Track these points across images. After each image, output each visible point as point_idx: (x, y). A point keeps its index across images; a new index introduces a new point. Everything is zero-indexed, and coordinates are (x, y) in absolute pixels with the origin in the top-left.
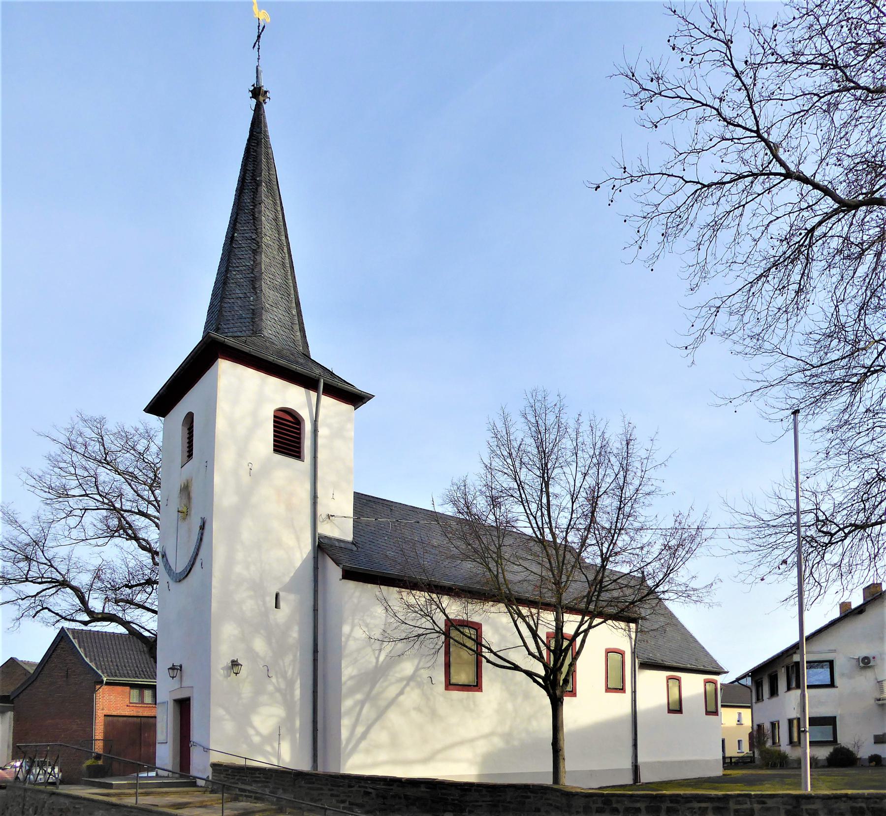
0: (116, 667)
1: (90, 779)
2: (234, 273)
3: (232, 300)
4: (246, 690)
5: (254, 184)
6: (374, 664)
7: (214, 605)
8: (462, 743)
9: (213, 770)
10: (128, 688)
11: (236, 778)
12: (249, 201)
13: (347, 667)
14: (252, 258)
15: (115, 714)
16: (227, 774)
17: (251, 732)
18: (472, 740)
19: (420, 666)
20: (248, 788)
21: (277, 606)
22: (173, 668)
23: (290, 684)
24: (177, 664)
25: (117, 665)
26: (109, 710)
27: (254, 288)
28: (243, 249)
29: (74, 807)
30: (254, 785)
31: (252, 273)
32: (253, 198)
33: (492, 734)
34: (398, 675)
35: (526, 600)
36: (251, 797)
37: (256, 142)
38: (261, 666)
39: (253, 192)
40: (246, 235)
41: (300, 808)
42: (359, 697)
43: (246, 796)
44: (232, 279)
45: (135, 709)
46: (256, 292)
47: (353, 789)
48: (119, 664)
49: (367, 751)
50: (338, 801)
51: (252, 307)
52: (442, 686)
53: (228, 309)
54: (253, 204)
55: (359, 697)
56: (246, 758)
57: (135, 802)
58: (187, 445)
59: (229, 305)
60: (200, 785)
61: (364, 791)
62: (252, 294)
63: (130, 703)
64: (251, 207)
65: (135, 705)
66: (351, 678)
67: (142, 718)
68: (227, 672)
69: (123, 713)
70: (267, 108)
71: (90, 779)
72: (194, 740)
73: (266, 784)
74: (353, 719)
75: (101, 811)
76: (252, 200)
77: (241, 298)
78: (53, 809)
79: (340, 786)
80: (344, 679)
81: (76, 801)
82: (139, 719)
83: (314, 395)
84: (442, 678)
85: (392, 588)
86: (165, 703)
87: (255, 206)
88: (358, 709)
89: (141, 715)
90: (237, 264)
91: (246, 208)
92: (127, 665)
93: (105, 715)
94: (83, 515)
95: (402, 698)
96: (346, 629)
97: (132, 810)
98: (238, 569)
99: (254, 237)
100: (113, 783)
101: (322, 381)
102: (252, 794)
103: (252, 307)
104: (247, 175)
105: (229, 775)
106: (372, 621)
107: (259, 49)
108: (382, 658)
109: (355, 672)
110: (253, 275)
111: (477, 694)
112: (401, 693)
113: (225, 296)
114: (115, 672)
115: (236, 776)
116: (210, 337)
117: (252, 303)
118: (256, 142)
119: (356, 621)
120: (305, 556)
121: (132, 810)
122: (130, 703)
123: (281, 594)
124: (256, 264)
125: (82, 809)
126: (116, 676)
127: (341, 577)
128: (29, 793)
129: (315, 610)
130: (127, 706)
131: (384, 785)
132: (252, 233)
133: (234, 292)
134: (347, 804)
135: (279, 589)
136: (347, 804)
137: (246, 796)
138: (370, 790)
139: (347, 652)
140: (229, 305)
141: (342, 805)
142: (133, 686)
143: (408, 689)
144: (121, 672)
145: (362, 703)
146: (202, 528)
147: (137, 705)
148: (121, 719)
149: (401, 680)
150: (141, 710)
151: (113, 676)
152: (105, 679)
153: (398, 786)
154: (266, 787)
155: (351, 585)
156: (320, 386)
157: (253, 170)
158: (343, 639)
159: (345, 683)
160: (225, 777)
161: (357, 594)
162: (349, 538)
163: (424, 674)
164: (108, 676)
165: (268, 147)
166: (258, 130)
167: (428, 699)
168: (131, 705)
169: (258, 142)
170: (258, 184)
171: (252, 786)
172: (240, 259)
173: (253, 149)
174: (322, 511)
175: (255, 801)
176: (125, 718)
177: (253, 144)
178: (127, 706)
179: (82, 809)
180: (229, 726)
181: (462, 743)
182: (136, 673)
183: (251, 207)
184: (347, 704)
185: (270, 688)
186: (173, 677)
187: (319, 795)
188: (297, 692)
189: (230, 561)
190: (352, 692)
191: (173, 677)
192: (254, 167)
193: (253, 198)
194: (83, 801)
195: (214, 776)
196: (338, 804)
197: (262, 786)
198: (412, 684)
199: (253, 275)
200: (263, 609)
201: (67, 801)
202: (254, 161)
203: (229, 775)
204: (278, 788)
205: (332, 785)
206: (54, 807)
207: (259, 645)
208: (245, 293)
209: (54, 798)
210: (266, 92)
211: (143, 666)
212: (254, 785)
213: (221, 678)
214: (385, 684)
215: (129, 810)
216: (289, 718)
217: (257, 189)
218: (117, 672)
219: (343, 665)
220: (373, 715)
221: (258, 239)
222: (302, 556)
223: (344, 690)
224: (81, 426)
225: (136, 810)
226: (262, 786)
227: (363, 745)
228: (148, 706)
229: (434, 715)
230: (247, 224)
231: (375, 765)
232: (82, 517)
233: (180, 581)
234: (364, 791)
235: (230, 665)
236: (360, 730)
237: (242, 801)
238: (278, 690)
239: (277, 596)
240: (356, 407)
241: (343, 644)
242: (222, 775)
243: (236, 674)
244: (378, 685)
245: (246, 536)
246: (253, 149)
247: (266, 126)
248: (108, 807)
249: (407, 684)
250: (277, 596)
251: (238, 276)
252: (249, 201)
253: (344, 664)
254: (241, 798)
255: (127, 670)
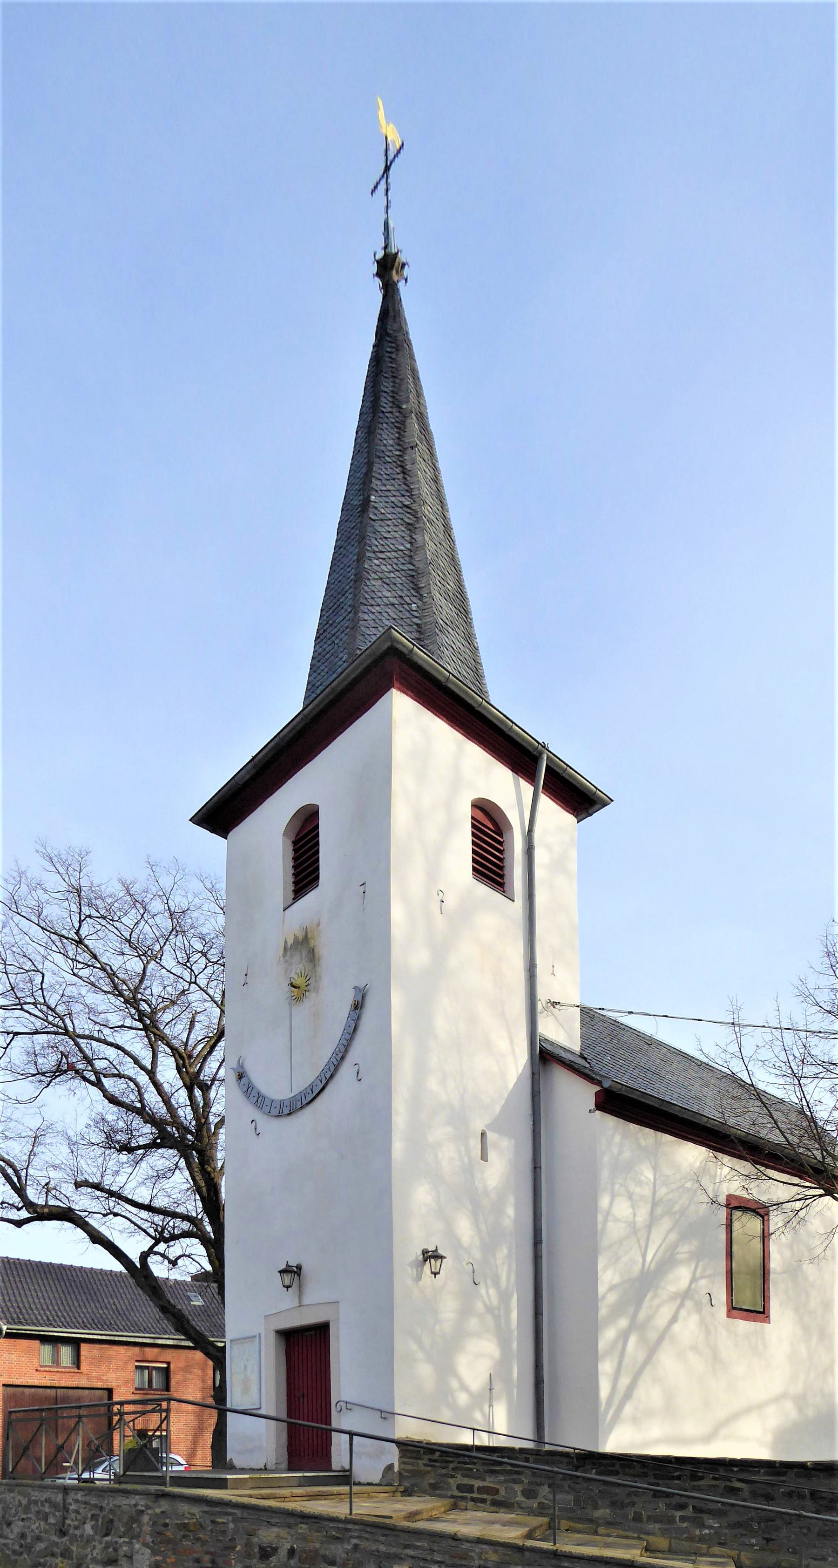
0: (18, 1310)
1: (146, 1474)
2: (376, 562)
3: (378, 608)
4: (448, 1309)
5: (397, 414)
6: (640, 1266)
7: (398, 1147)
8: (748, 1410)
9: (401, 1451)
10: (36, 1343)
11: (451, 1466)
12: (391, 442)
13: (605, 1268)
14: (408, 538)
15: (19, 1383)
16: (430, 1460)
17: (455, 1384)
18: (760, 1407)
19: (698, 1274)
20: (477, 1484)
21: (484, 1157)
22: (286, 1271)
23: (504, 1297)
24: (293, 1263)
25: (18, 1307)
26: (10, 1376)
27: (417, 589)
28: (389, 523)
29: (213, 1522)
30: (488, 1479)
31: (411, 563)
32: (398, 438)
33: (783, 1396)
34: (672, 1289)
35: (168, 1315)
36: (483, 1501)
37: (393, 345)
38: (464, 1264)
39: (397, 428)
40: (393, 499)
41: (591, 1521)
42: (623, 1323)
43: (473, 1500)
44: (375, 573)
45: (48, 1375)
46: (421, 595)
47: (701, 1483)
48: (21, 1305)
49: (635, 1420)
50: (669, 1506)
51: (415, 620)
52: (724, 1310)
53: (372, 624)
54: (399, 448)
55: (623, 1323)
56: (474, 1429)
57: (348, 1512)
58: (292, 872)
59: (373, 617)
60: (363, 1480)
61: (726, 1487)
62: (414, 599)
63: (41, 1366)
64: (398, 453)
65: (47, 1369)
66: (612, 1288)
67: (59, 1390)
68: (417, 1271)
69: (31, 1382)
70: (405, 291)
71: (146, 1474)
72: (345, 1397)
73: (515, 1476)
74: (616, 1360)
75: (275, 1529)
76: (396, 441)
77: (393, 605)
78: (166, 1525)
79: (673, 1478)
80: (601, 1290)
81: (218, 1509)
82: (55, 1390)
83: (527, 789)
84: (721, 1296)
85: (660, 1133)
86: (255, 1337)
87: (403, 450)
88: (620, 1346)
89: (57, 1385)
90: (380, 547)
91: (387, 453)
92: (33, 1307)
93: (4, 1385)
94: (8, 1045)
95: (676, 1327)
96: (604, 1201)
97: (350, 1526)
98: (433, 1084)
99: (407, 503)
100: (229, 1477)
101: (545, 758)
102: (485, 1496)
103: (415, 620)
104: (383, 399)
105: (435, 1461)
106: (638, 1190)
107: (387, 190)
108: (649, 1257)
109: (617, 1280)
110: (412, 567)
111: (766, 1325)
112: (674, 1319)
113: (364, 601)
114: (18, 1318)
115: (452, 1462)
116: (393, 640)
117: (416, 614)
118: (393, 345)
119: (617, 1187)
120: (520, 1070)
121: (350, 1526)
122: (41, 1366)
123: (491, 1136)
124: (414, 549)
125: (231, 1526)
126: (20, 1323)
127: (593, 1107)
128: (72, 1496)
129: (536, 1168)
130: (37, 1370)
131: (766, 1474)
132: (403, 496)
133: (379, 594)
134: (689, 1512)
135: (486, 1126)
136: (689, 1512)
137: (473, 1500)
138: (738, 1485)
139: (605, 1242)
140: (373, 617)
141: (678, 1514)
142: (45, 1339)
143: (683, 1313)
144: (27, 1317)
145: (624, 1336)
146: (358, 1007)
147: (52, 1369)
148: (27, 1391)
149: (673, 1297)
150: (56, 1377)
151: (15, 1323)
152: (4, 1328)
153: (798, 1475)
154: (515, 1481)
155: (610, 1122)
156: (541, 767)
157: (393, 392)
158: (600, 1218)
159: (604, 1297)
160: (425, 1465)
161: (617, 1139)
162: (576, 1047)
163: (703, 1284)
164: (8, 1322)
165: (412, 357)
166: (396, 327)
167: (708, 1332)
168: (42, 1369)
169: (398, 345)
170: (404, 416)
171: (484, 1480)
172: (386, 538)
173: (390, 357)
174: (543, 995)
175: (494, 1509)
176: (33, 1390)
177: (389, 350)
178: (37, 1370)
179: (231, 1526)
180: (425, 1371)
181: (748, 1410)
182: (48, 1319)
183: (398, 453)
184: (608, 1336)
185: (479, 1306)
186: (288, 1287)
187: (629, 1494)
188: (514, 1315)
189: (421, 1069)
190: (616, 1311)
191: (288, 1287)
192: (394, 386)
193: (398, 438)
194: (230, 1510)
195: (404, 1463)
196: (671, 1512)
197: (505, 1481)
198: (689, 1304)
199: (412, 567)
200: (466, 1160)
201: (196, 1510)
202: (393, 377)
203: (435, 1461)
204: (541, 1484)
205: (656, 1476)
206: (167, 1521)
207: (465, 1228)
208: (401, 597)
209: (164, 1505)
210: (403, 265)
211: (56, 1308)
212: (488, 1479)
213: (409, 1282)
214: (656, 1302)
215: (341, 1526)
216: (503, 1363)
217: (403, 423)
218: (21, 1317)
219: (600, 1266)
220: (641, 1356)
221: (414, 506)
222: (517, 1072)
223: (603, 1311)
224: (37, 868)
225: (357, 1527)
226: (505, 1481)
227: (628, 1409)
228: (68, 1370)
229: (716, 1360)
230: (392, 481)
231: (646, 1444)
232: (6, 1048)
233: (289, 1114)
234: (726, 1487)
235: (421, 1258)
236: (624, 1381)
237: (466, 1509)
238: (489, 1309)
239: (483, 1134)
240: (580, 817)
241: (599, 1227)
242: (420, 1462)
243: (435, 1274)
244: (646, 1303)
245: (441, 1024)
246: (390, 357)
247: (406, 324)
248: (292, 1520)
249: (681, 1305)
250: (483, 1134)
251: (384, 568)
252: (391, 442)
253: (601, 1263)
254: (462, 1504)
255: (34, 1313)
